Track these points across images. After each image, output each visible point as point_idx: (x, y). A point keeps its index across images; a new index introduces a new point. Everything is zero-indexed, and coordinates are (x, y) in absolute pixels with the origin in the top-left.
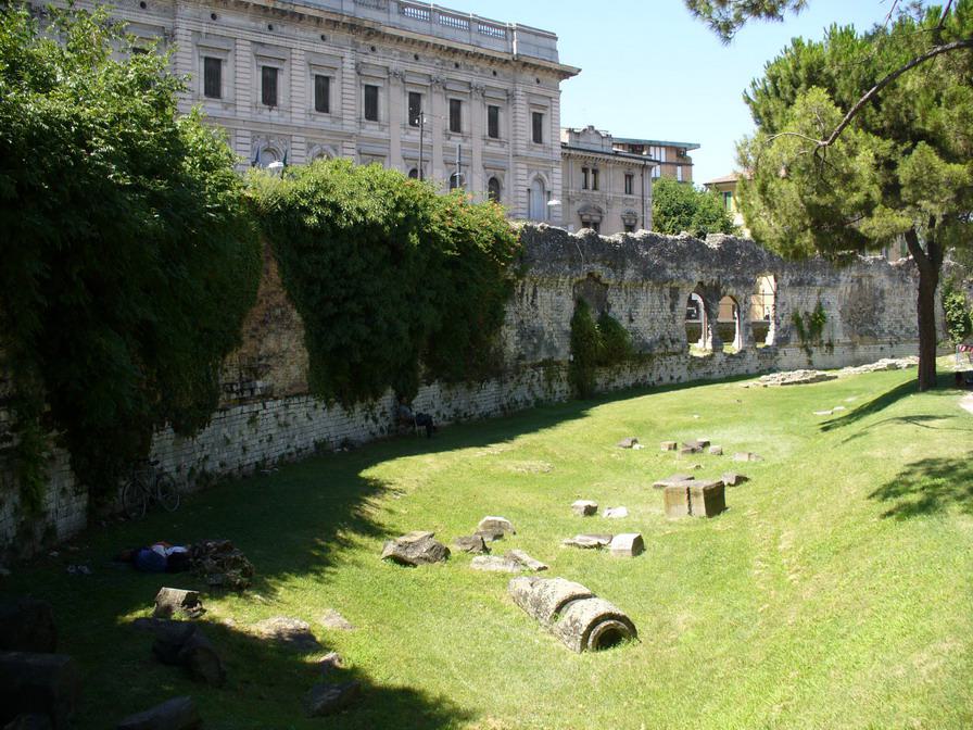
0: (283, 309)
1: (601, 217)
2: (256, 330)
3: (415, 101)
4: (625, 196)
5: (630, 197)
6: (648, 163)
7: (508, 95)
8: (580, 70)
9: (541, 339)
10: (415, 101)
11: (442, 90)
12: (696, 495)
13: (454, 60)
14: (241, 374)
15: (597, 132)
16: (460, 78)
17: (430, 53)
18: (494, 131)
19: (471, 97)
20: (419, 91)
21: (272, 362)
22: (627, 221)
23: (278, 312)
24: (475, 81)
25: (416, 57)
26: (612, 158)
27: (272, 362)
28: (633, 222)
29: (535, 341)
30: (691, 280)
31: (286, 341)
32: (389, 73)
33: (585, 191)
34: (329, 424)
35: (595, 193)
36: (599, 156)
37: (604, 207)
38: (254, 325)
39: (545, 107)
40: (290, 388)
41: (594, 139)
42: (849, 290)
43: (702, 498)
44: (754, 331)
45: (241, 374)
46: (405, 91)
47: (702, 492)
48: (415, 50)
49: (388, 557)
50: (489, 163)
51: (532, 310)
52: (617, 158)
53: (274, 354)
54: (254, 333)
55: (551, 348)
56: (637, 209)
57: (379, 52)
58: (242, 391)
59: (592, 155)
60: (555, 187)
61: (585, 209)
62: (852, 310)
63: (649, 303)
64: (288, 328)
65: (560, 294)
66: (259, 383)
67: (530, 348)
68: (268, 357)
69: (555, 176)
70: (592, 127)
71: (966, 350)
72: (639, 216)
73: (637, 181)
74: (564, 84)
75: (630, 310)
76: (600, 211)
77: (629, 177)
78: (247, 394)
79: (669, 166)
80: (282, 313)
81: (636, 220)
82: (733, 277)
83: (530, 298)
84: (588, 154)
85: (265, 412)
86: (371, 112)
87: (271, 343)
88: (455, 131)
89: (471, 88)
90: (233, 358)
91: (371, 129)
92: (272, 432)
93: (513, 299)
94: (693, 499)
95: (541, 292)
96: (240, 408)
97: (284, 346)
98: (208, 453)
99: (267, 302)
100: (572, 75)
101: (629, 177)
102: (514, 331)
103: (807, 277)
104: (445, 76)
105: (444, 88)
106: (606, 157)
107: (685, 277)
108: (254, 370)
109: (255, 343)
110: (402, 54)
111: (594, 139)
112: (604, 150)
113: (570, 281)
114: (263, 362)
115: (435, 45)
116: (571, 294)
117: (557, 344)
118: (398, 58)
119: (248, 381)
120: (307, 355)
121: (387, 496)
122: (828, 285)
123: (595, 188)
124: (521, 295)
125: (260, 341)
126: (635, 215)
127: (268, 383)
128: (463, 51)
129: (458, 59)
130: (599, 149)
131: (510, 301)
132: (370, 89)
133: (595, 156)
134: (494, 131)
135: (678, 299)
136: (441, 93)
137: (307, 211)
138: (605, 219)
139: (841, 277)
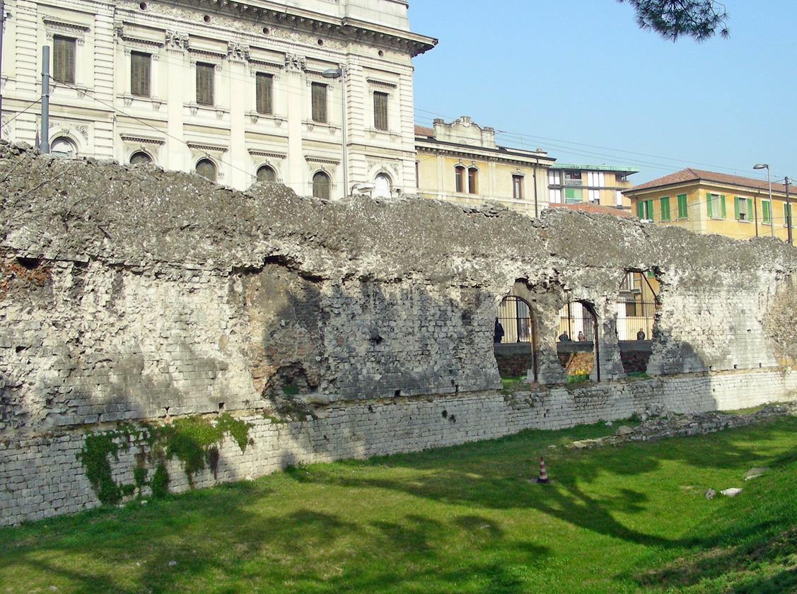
4: (515, 201)
8: (436, 41)
18: (320, 115)
20: (211, 60)
24: (293, 51)
30: (501, 275)
33: (460, 195)
35: (473, 196)
42: (773, 292)
44: (622, 354)
49: (429, 556)
50: (314, 152)
52: (501, 156)
60: (407, 183)
62: (778, 320)
63: (416, 311)
69: (406, 170)
71: (727, 425)
79: (608, 191)
82: (581, 272)
86: (141, 85)
88: (265, 113)
91: (141, 108)
103: (708, 273)
105: (247, 58)
121: (137, 578)
122: (740, 286)
123: (472, 190)
130: (478, 144)
133: (203, 9)
134: (320, 115)
139: (760, 273)
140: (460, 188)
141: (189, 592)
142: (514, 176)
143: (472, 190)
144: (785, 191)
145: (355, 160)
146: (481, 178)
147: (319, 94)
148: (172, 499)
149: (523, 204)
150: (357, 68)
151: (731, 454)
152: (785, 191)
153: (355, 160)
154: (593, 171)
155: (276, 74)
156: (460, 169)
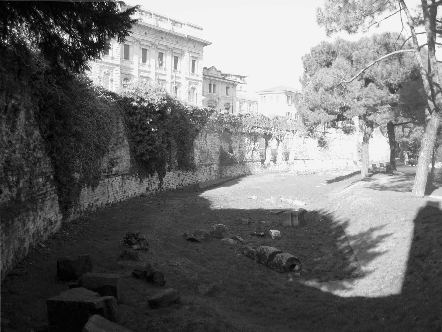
0: (122, 139)
1: (216, 105)
2: (113, 147)
3: (144, 51)
4: (226, 96)
5: (228, 96)
6: (235, 83)
7: (182, 52)
8: (211, 43)
9: (208, 154)
10: (144, 51)
11: (156, 48)
12: (295, 216)
13: (161, 36)
14: (108, 165)
15: (215, 69)
16: (163, 44)
17: (151, 32)
19: (167, 52)
20: (146, 48)
21: (118, 160)
22: (226, 107)
23: (121, 140)
24: (169, 45)
25: (146, 33)
26: (221, 80)
27: (118, 160)
28: (229, 107)
29: (206, 155)
31: (123, 152)
32: (134, 40)
33: (210, 94)
34: (136, 186)
35: (214, 94)
36: (216, 79)
37: (217, 100)
38: (113, 145)
39: (197, 58)
40: (124, 172)
41: (214, 72)
43: (297, 217)
45: (108, 165)
46: (141, 48)
47: (297, 215)
48: (145, 31)
51: (205, 142)
52: (223, 80)
53: (119, 157)
54: (113, 149)
55: (211, 159)
56: (231, 102)
57: (148, 35)
58: (108, 172)
59: (213, 78)
61: (210, 101)
64: (124, 147)
65: (215, 136)
66: (114, 169)
67: (204, 157)
68: (117, 158)
70: (214, 67)
72: (231, 104)
73: (231, 90)
74: (205, 48)
75: (240, 144)
76: (216, 102)
77: (228, 88)
78: (110, 174)
80: (122, 141)
81: (230, 106)
83: (204, 137)
84: (212, 78)
85: (115, 181)
87: (118, 153)
89: (167, 48)
90: (105, 158)
92: (117, 189)
93: (198, 137)
94: (294, 218)
95: (208, 135)
96: (108, 179)
97: (122, 154)
98: (97, 198)
99: (117, 136)
100: (208, 45)
101: (228, 88)
102: (199, 151)
104: (157, 43)
105: (157, 48)
106: (219, 80)
107: (74, 99)
108: (113, 163)
109: (113, 152)
110: (140, 32)
111: (214, 72)
112: (218, 77)
113: (219, 131)
114: (115, 161)
115: (154, 29)
116: (219, 136)
117: (213, 157)
118: (138, 34)
119: (111, 168)
120: (130, 158)
123: (214, 92)
124: (201, 136)
125: (115, 152)
126: (229, 104)
127: (117, 169)
128: (165, 32)
129: (163, 36)
130: (216, 76)
131: (197, 139)
132: (126, 46)
135: (257, 140)
136: (155, 49)
137: (132, 100)
138: (217, 105)
140: (210, 92)
141: (438, 165)
142: (227, 88)
143: (214, 92)
144: (400, 12)
145: (329, 133)
146: (217, 88)
147: (176, 60)
148: (427, 165)
149: (229, 98)
150: (187, 51)
151: (220, 224)
152: (400, 12)
153: (329, 133)
154: (232, 75)
155: (164, 53)
156: (210, 85)
